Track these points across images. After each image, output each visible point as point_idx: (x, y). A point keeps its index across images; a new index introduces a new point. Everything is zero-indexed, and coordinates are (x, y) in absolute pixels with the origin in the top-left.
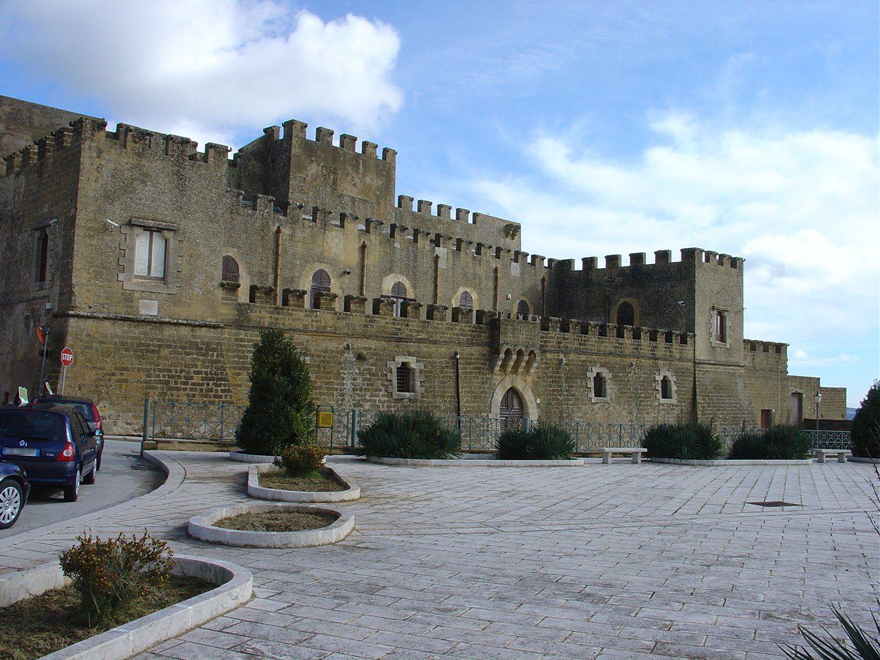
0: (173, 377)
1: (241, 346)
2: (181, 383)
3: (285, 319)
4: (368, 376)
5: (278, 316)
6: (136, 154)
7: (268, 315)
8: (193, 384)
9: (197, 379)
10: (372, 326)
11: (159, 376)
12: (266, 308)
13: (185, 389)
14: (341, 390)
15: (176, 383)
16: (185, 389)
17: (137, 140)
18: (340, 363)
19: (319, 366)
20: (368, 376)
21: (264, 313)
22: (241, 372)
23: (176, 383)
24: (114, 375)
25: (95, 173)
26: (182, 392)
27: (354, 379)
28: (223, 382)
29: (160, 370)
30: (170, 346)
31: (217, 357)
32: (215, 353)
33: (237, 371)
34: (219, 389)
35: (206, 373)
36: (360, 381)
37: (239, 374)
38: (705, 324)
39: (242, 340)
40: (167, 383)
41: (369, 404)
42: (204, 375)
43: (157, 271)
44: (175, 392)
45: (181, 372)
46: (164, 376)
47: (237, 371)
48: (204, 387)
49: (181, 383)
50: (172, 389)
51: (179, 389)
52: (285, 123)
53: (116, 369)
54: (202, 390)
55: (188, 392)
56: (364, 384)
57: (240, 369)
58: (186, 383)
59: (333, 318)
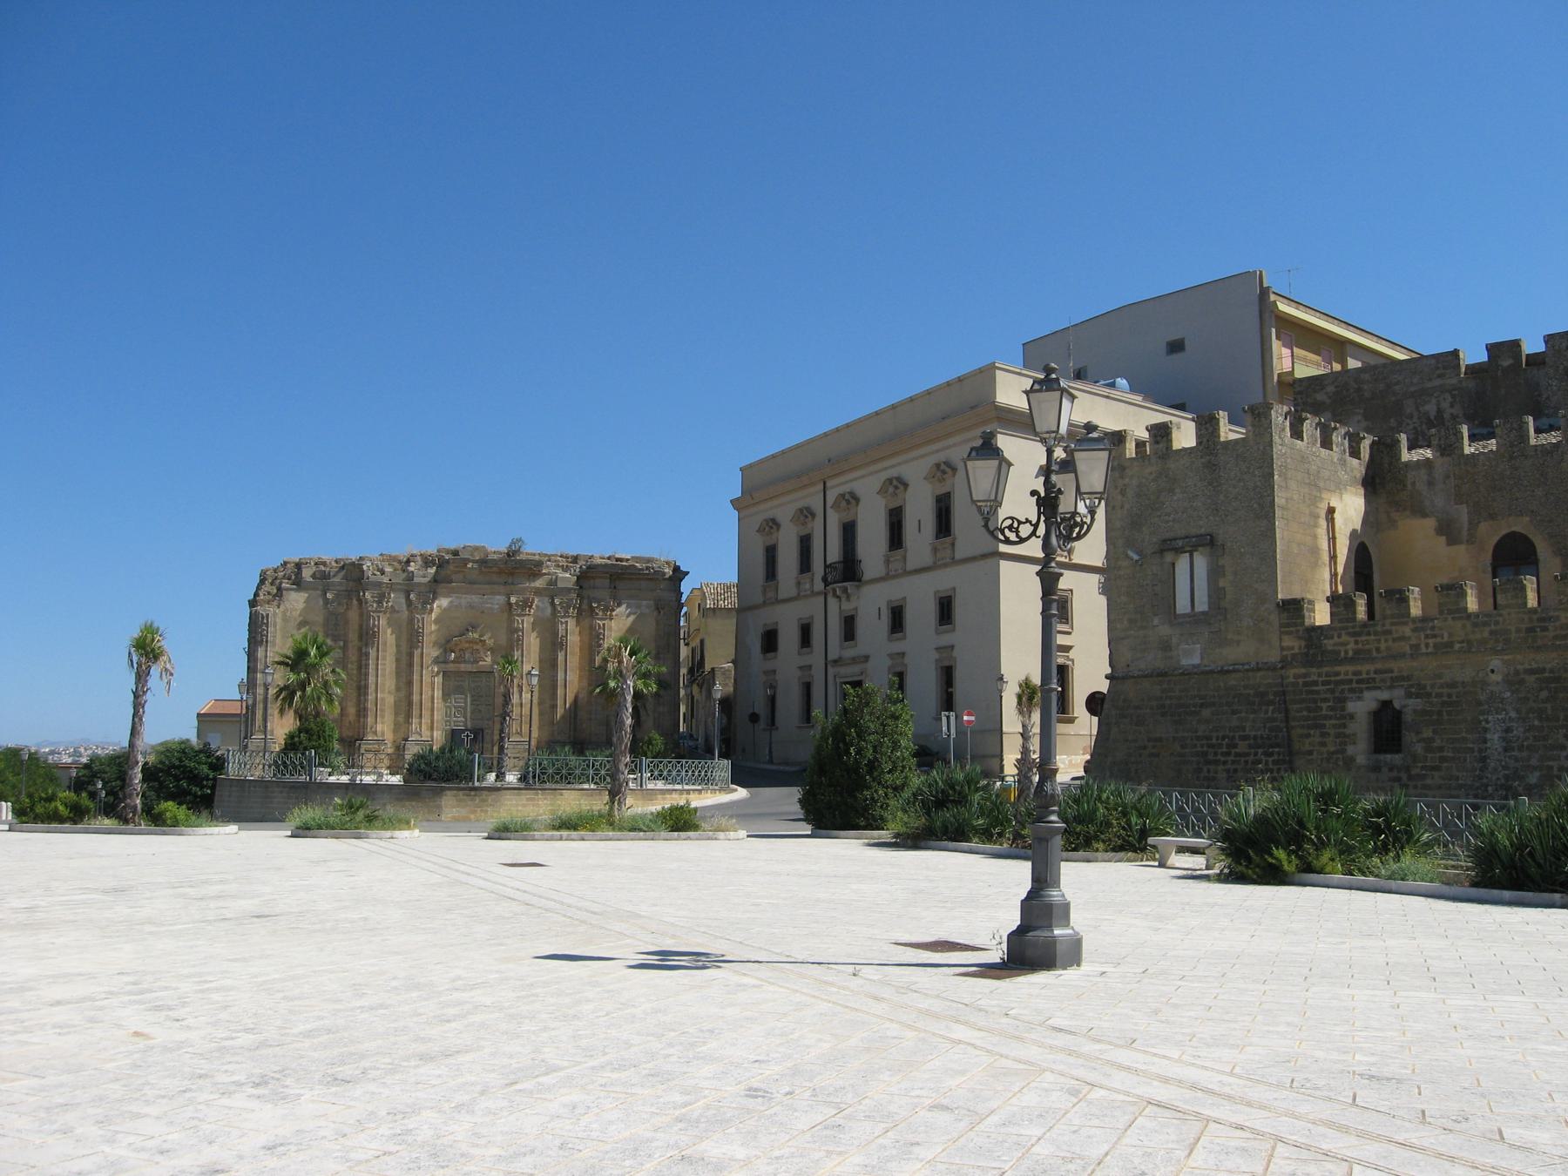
0: (1213, 746)
1: (1312, 692)
2: (1222, 754)
3: (1380, 640)
4: (1536, 723)
5: (1367, 638)
6: (1159, 457)
7: (1352, 639)
8: (1237, 755)
9: (1242, 747)
10: (1545, 629)
11: (1195, 746)
12: (1347, 628)
13: (1225, 763)
14: (1480, 751)
15: (1216, 754)
16: (1225, 763)
17: (1159, 438)
18: (1480, 703)
19: (1440, 713)
20: (1536, 723)
21: (1345, 638)
22: (1312, 732)
23: (1216, 754)
24: (1145, 748)
25: (1120, 497)
26: (1220, 768)
27: (1508, 730)
28: (1277, 750)
29: (1198, 738)
30: (1213, 704)
31: (1272, 713)
32: (1271, 708)
33: (1305, 731)
34: (1270, 759)
35: (1255, 738)
36: (1518, 731)
37: (1308, 736)
38: (1065, 854)
39: (1315, 683)
40: (1205, 754)
41: (1537, 774)
42: (1252, 741)
43: (1202, 605)
44: (1212, 767)
45: (1223, 738)
46: (1202, 746)
47: (1305, 731)
48: (1252, 758)
49: (1222, 754)
50: (1208, 762)
51: (1216, 762)
52: (1152, 426)
53: (1149, 740)
54: (1246, 762)
55: (1229, 766)
56: (1527, 738)
57: (1309, 727)
58: (1228, 754)
59: (1464, 626)
